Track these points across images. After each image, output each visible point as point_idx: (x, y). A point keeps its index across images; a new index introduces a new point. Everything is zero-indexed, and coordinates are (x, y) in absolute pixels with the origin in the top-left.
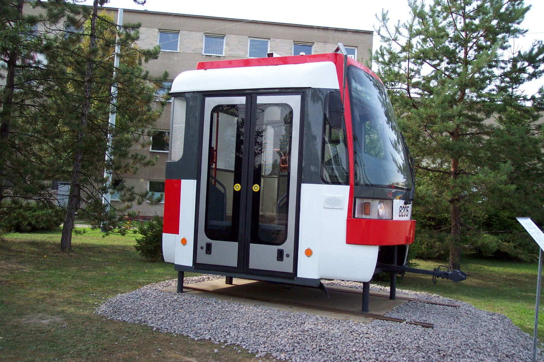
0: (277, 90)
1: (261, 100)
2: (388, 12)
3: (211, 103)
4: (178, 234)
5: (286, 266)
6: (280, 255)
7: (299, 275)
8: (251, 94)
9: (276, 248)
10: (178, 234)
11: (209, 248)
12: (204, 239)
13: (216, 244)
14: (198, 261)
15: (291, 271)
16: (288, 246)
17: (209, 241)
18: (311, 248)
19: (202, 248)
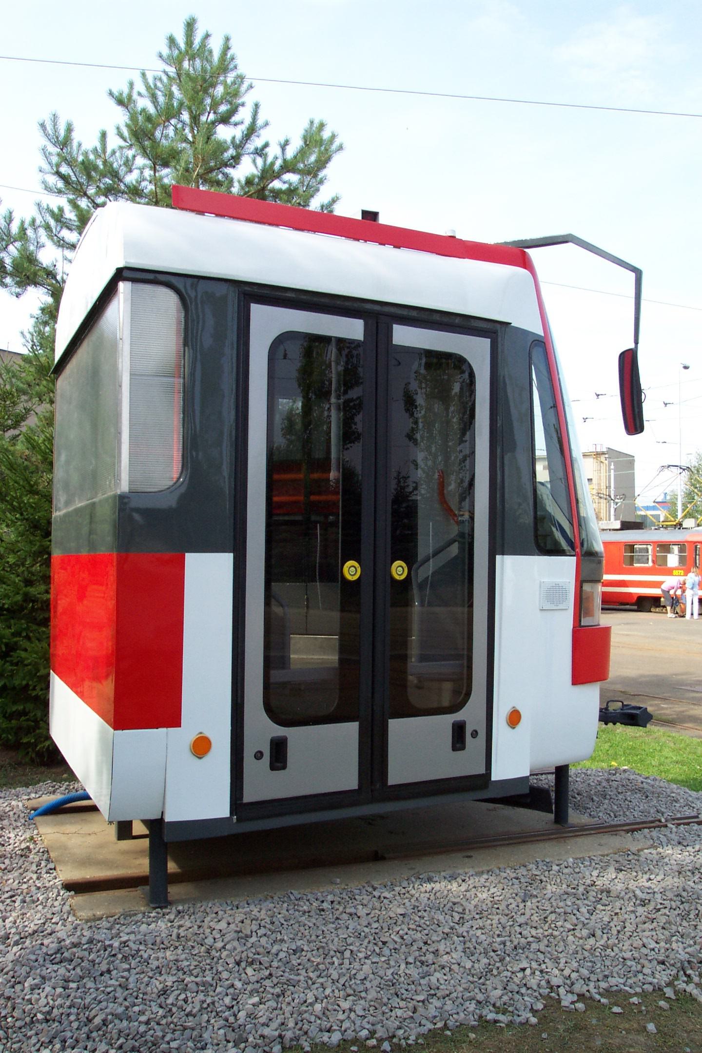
0: (414, 314)
1: (404, 336)
2: (267, 124)
3: (267, 324)
4: (178, 725)
5: (466, 764)
6: (459, 734)
7: (495, 777)
8: (380, 315)
9: (448, 720)
10: (178, 725)
11: (278, 754)
12: (261, 729)
13: (298, 738)
14: (249, 796)
15: (482, 770)
16: (471, 713)
17: (280, 731)
18: (208, 734)
19: (475, 734)
